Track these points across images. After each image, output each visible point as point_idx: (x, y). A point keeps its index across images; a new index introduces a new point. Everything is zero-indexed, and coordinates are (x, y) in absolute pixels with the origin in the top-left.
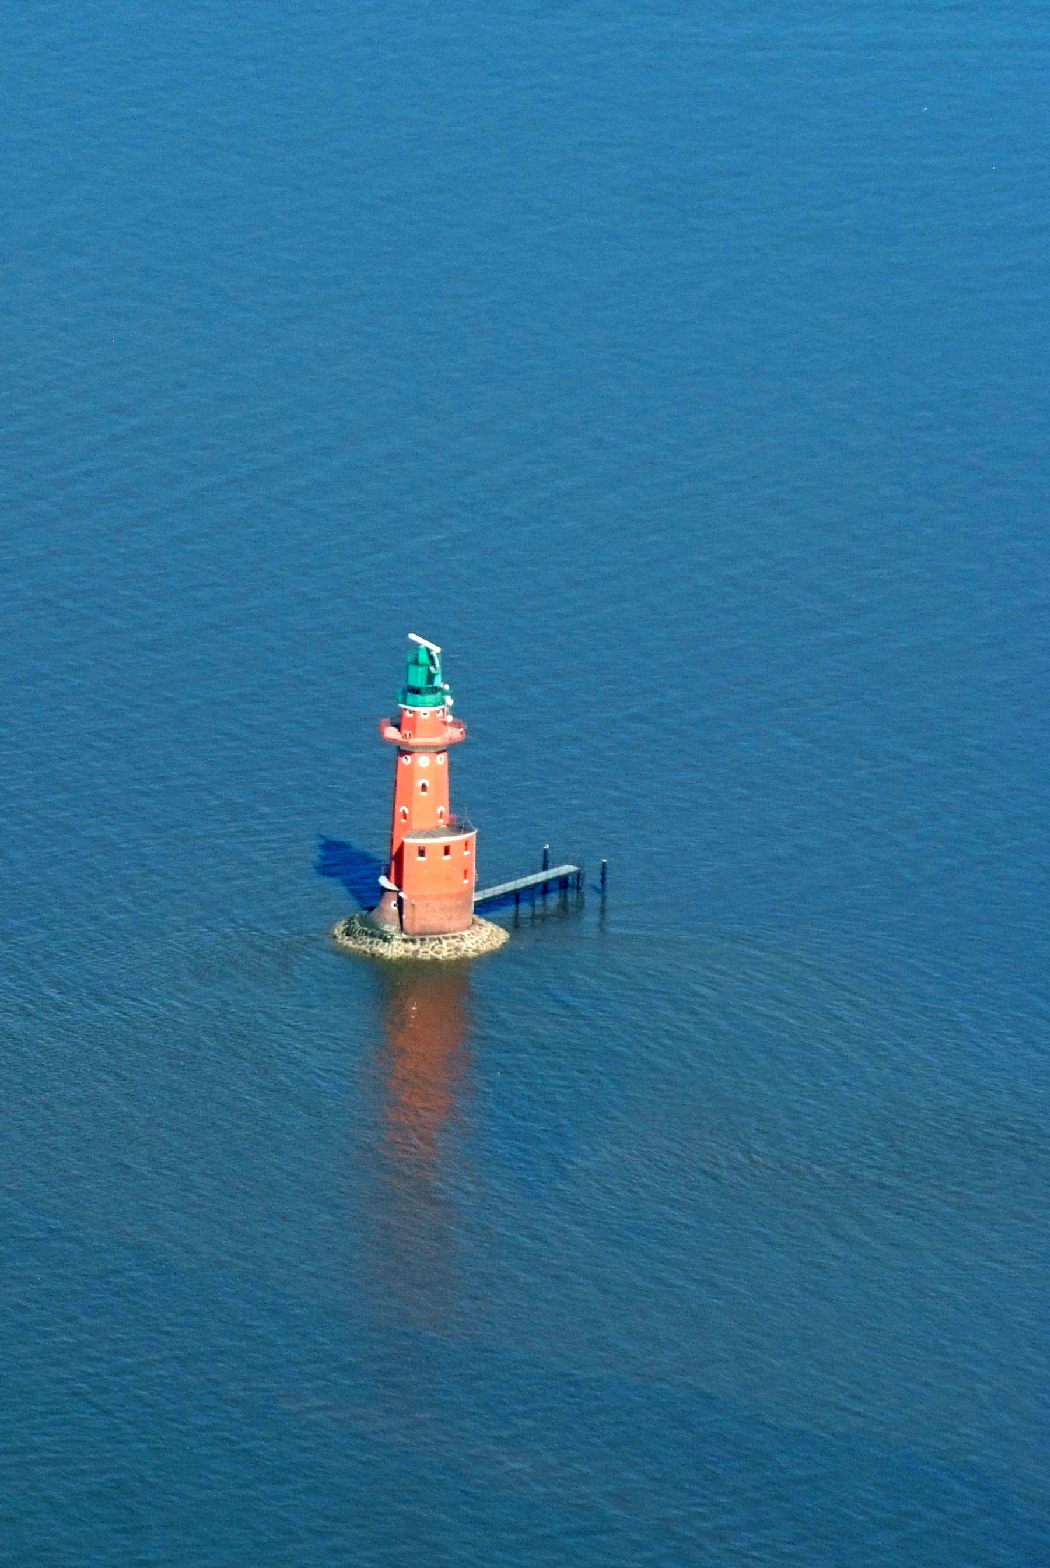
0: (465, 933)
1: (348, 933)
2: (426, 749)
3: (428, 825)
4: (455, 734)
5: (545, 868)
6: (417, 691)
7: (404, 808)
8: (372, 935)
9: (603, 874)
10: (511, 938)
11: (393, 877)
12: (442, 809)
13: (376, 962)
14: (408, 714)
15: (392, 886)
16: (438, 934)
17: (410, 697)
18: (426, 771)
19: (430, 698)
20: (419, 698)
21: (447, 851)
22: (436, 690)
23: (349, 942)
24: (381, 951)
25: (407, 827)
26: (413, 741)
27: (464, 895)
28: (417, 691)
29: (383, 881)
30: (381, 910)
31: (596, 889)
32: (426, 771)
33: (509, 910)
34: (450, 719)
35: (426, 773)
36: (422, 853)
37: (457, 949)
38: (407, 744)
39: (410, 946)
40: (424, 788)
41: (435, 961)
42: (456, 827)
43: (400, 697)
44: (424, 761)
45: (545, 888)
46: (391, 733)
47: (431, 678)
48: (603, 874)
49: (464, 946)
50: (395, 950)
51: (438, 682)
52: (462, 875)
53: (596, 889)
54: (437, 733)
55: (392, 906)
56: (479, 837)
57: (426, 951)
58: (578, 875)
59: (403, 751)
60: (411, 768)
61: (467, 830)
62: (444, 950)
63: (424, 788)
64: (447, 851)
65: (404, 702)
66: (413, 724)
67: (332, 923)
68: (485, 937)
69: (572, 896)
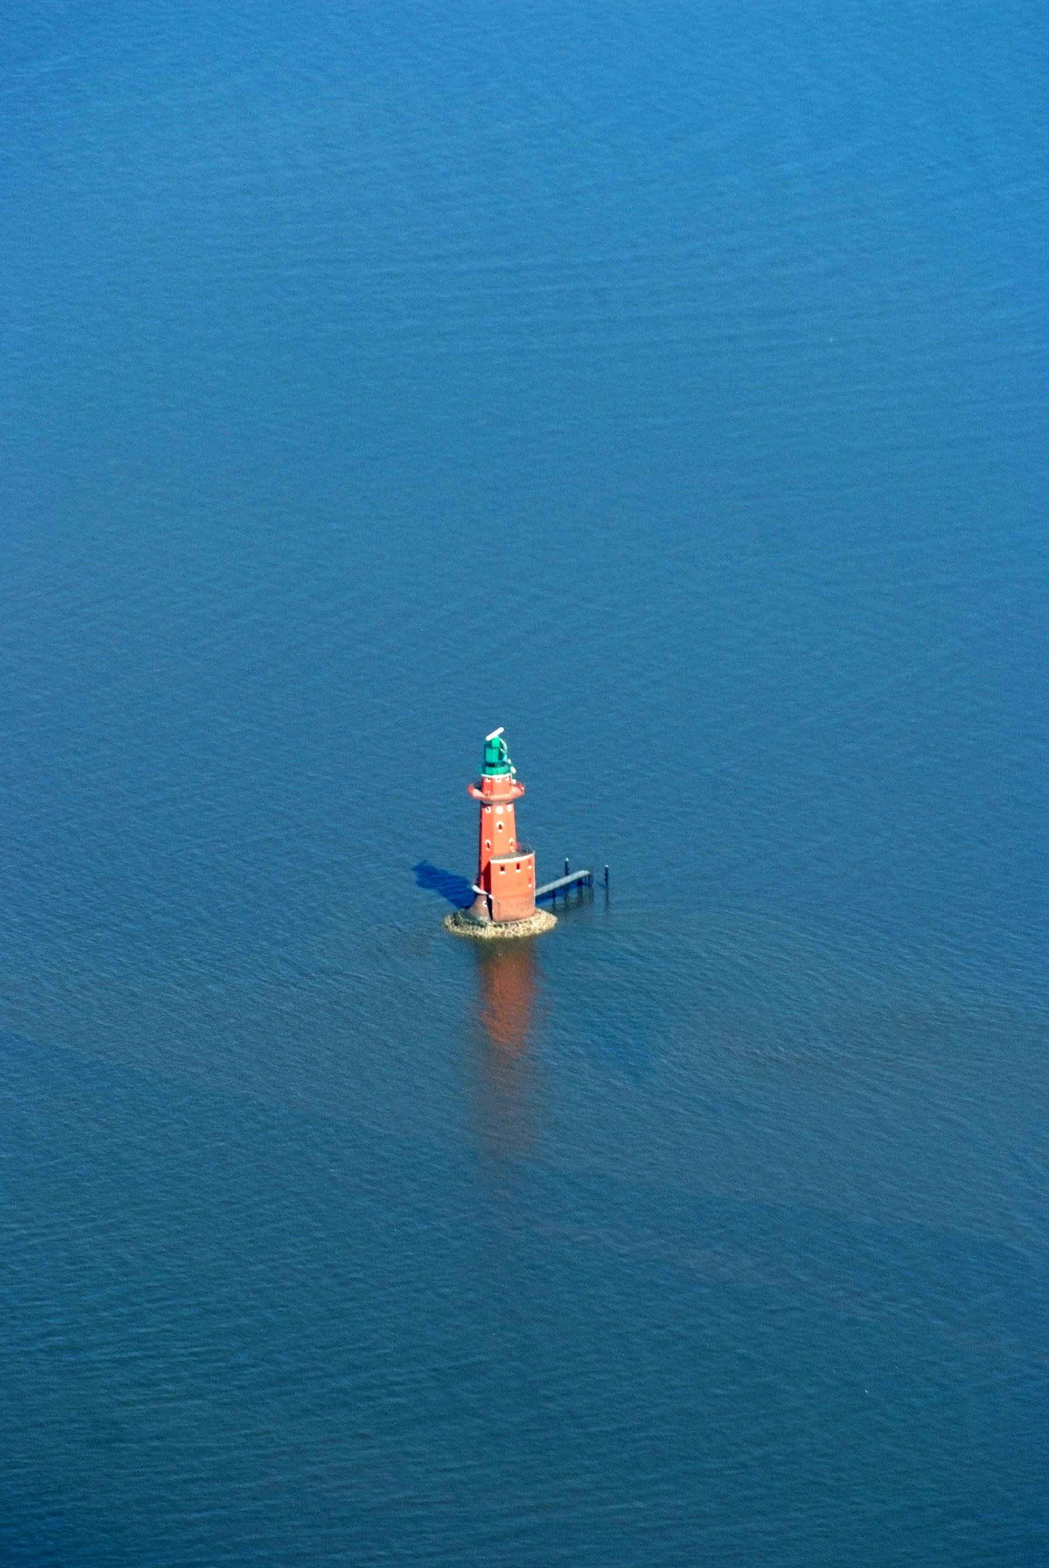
0: (532, 919)
1: (456, 923)
2: (500, 802)
3: (504, 851)
4: (515, 791)
5: (567, 874)
6: (492, 765)
7: (488, 841)
8: (473, 924)
9: (606, 875)
10: (559, 920)
11: (482, 886)
12: (512, 840)
13: (477, 943)
14: (488, 781)
15: (482, 891)
16: (516, 920)
17: (488, 769)
18: (501, 816)
19: (501, 769)
20: (494, 769)
21: (518, 867)
22: (504, 764)
23: (457, 930)
24: (480, 934)
25: (491, 853)
26: (493, 797)
27: (531, 892)
28: (492, 765)
29: (475, 888)
30: (476, 908)
31: (601, 885)
32: (501, 816)
33: (550, 902)
34: (514, 781)
35: (500, 817)
36: (502, 869)
37: (529, 929)
38: (489, 800)
39: (499, 929)
40: (500, 827)
41: (516, 938)
42: (523, 851)
43: (480, 770)
44: (499, 810)
45: (566, 888)
46: (476, 793)
47: (501, 756)
48: (606, 875)
49: (532, 927)
50: (489, 932)
51: (505, 758)
52: (527, 880)
53: (601, 885)
54: (507, 791)
55: (484, 904)
56: (537, 857)
57: (510, 932)
58: (590, 876)
59: (484, 804)
60: (491, 816)
61: (529, 852)
62: (520, 931)
63: (500, 827)
64: (518, 867)
65: (484, 772)
66: (491, 786)
67: (444, 916)
68: (543, 921)
69: (585, 890)
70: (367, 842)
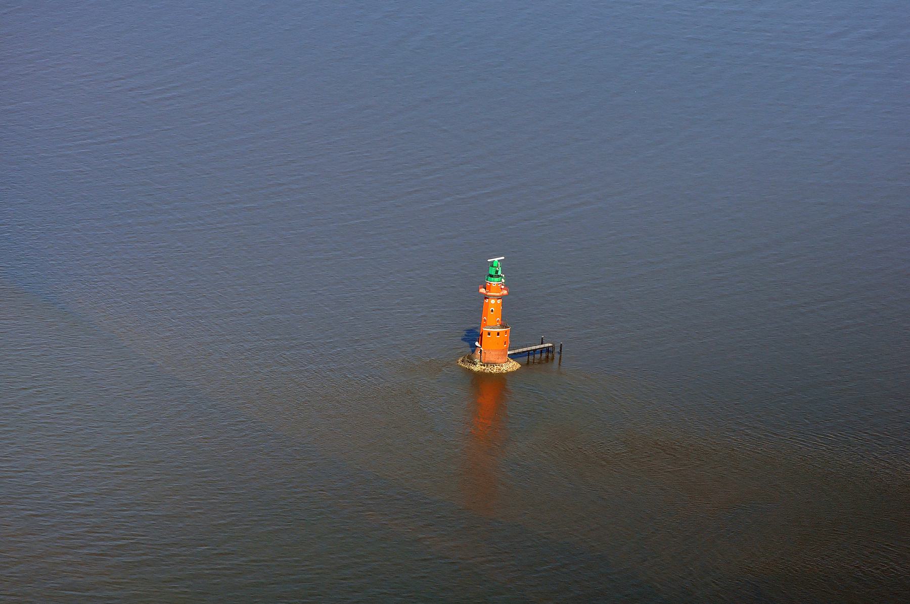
6: (492, 276)
18: (494, 304)
22: (499, 276)
28: (492, 276)
32: (494, 304)
42: (502, 326)
46: (482, 290)
50: (477, 368)
51: (499, 273)
57: (488, 369)
68: (512, 366)
70: (191, 583)
